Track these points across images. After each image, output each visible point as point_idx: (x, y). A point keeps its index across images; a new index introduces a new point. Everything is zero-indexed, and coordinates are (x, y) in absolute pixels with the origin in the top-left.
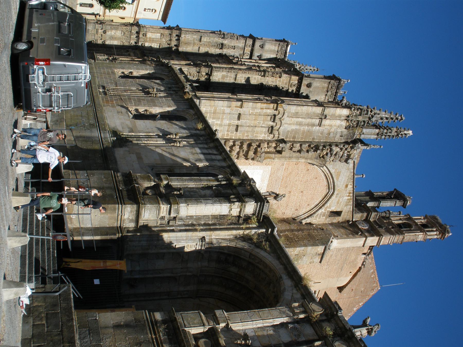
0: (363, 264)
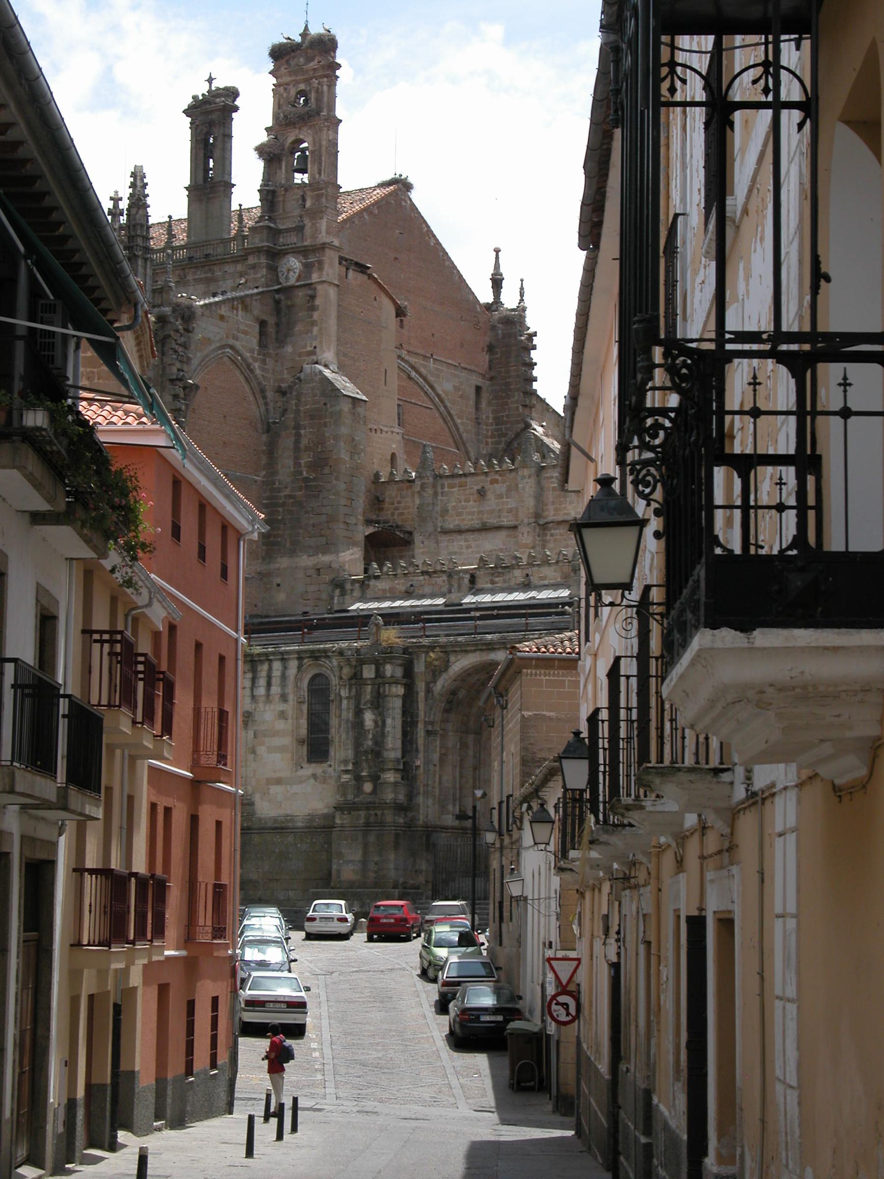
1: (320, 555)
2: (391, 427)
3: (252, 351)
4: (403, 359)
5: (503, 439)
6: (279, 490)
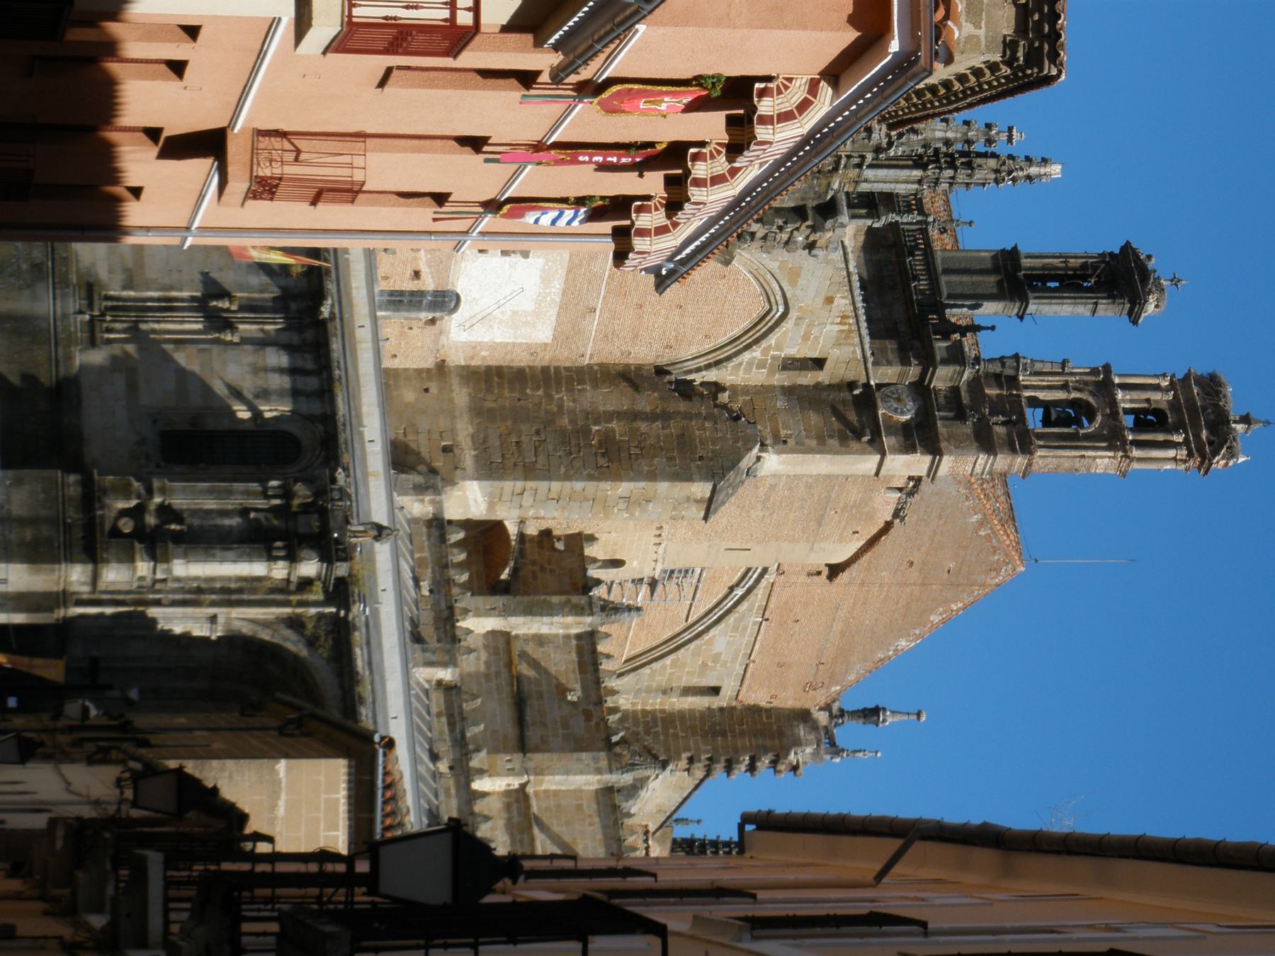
0: (896, 514)
1: (473, 453)
2: (664, 559)
3: (779, 347)
4: (761, 576)
5: (641, 729)
6: (570, 390)
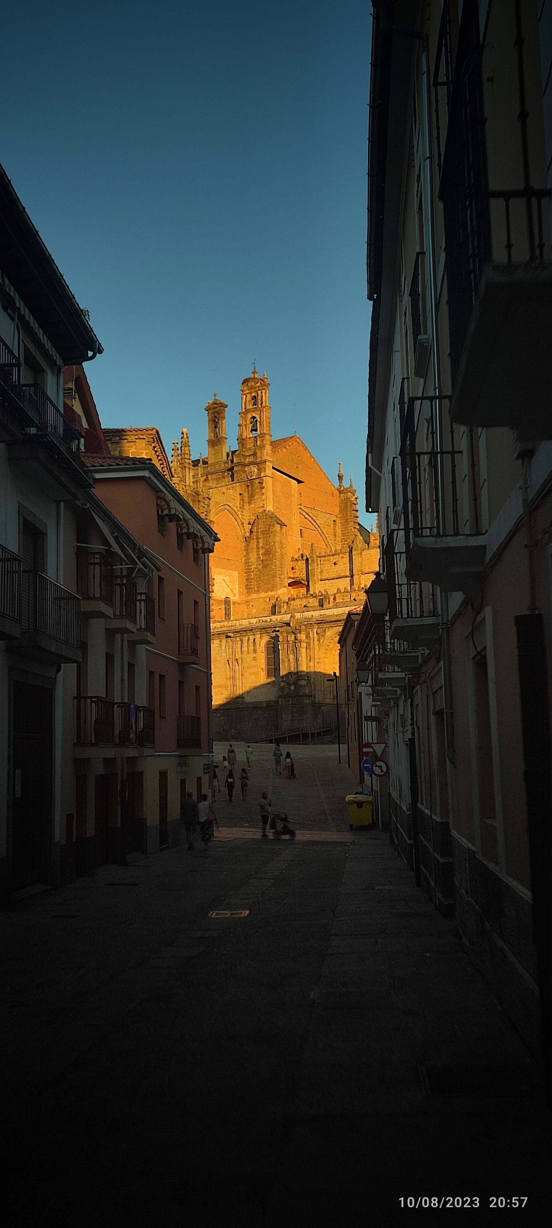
1: (269, 592)
6: (251, 566)
